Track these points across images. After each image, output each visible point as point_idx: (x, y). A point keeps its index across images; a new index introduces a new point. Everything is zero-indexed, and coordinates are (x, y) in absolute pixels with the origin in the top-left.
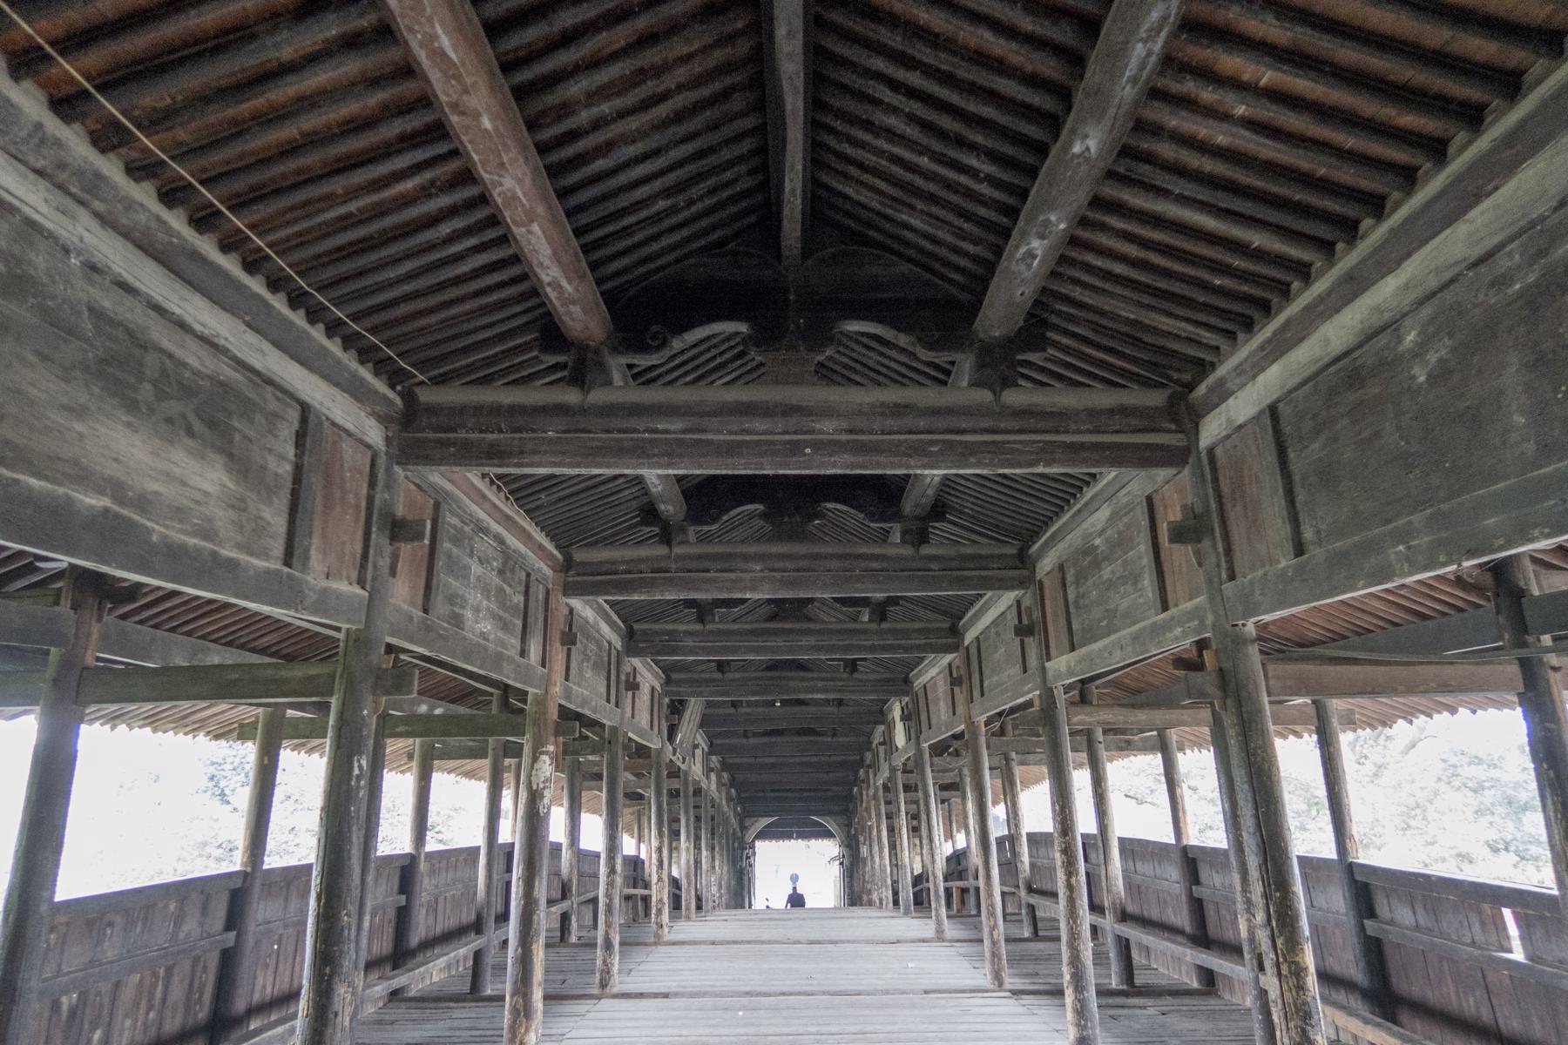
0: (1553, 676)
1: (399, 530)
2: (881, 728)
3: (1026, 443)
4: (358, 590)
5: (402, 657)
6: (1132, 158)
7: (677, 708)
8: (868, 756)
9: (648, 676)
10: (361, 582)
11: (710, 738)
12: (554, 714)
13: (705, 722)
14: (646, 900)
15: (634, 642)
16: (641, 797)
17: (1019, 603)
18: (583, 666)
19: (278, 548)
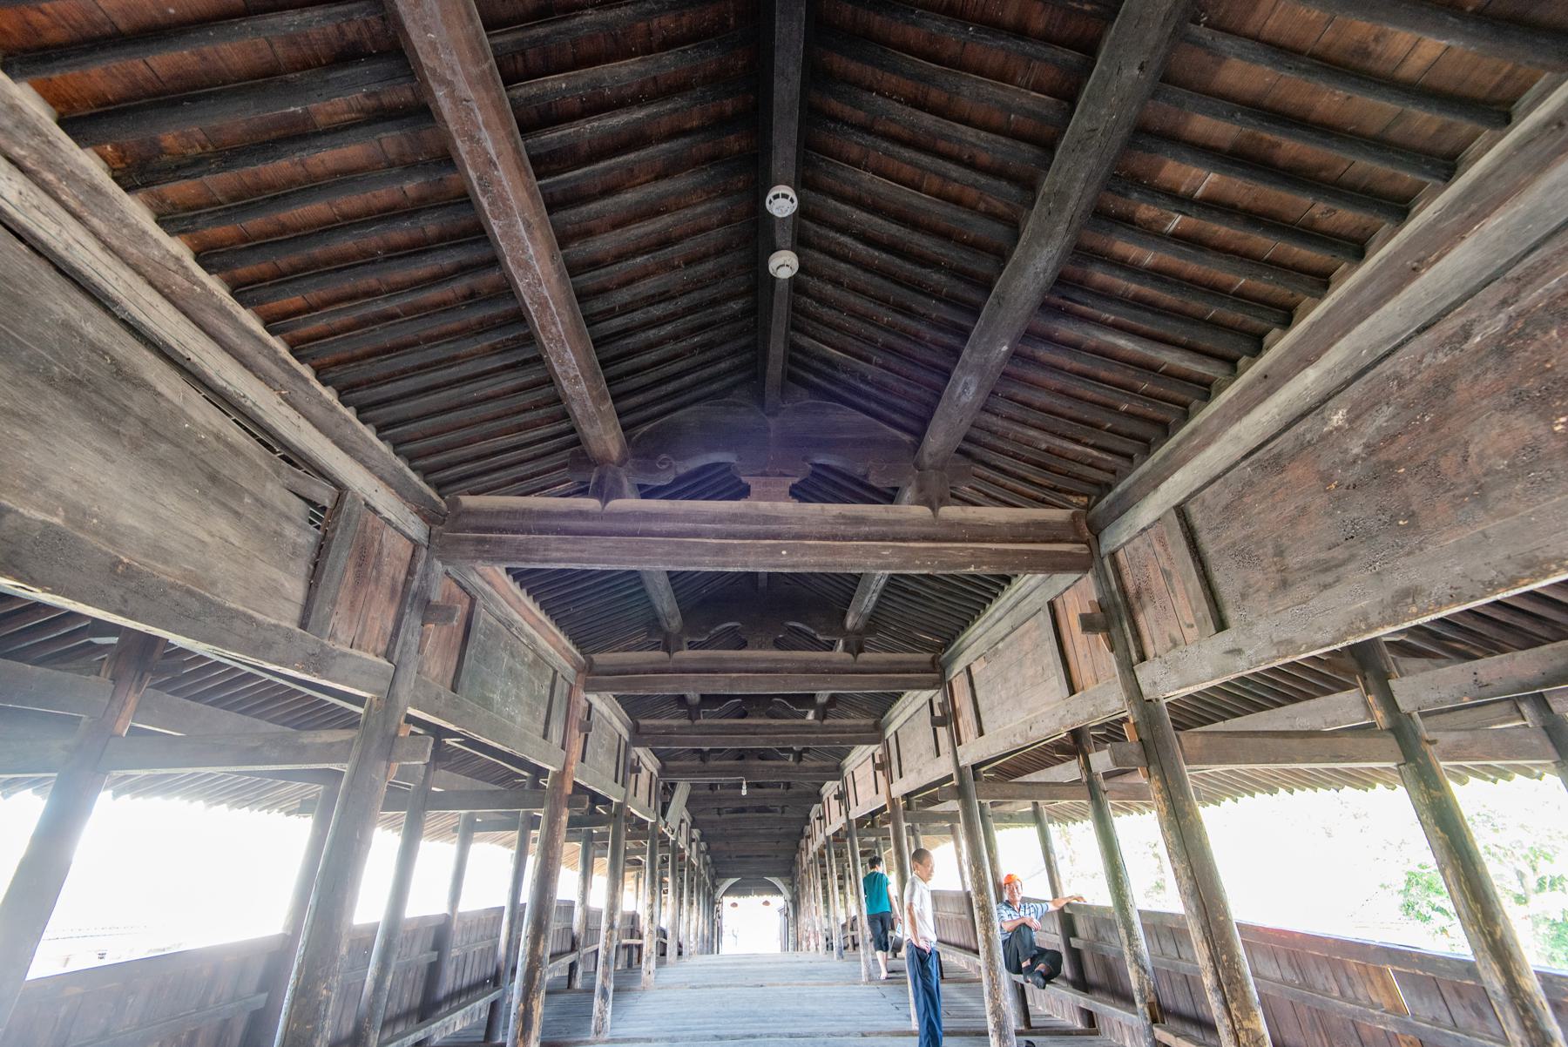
0: (1431, 749)
1: (429, 610)
2: (817, 807)
3: (961, 550)
4: (384, 662)
5: (448, 741)
6: (1066, 289)
7: (669, 789)
8: (808, 828)
9: (648, 762)
10: (388, 655)
11: (692, 814)
12: (569, 789)
13: (691, 802)
14: (640, 947)
15: (638, 735)
16: (640, 862)
17: (931, 701)
18: (596, 746)
19: (295, 612)
